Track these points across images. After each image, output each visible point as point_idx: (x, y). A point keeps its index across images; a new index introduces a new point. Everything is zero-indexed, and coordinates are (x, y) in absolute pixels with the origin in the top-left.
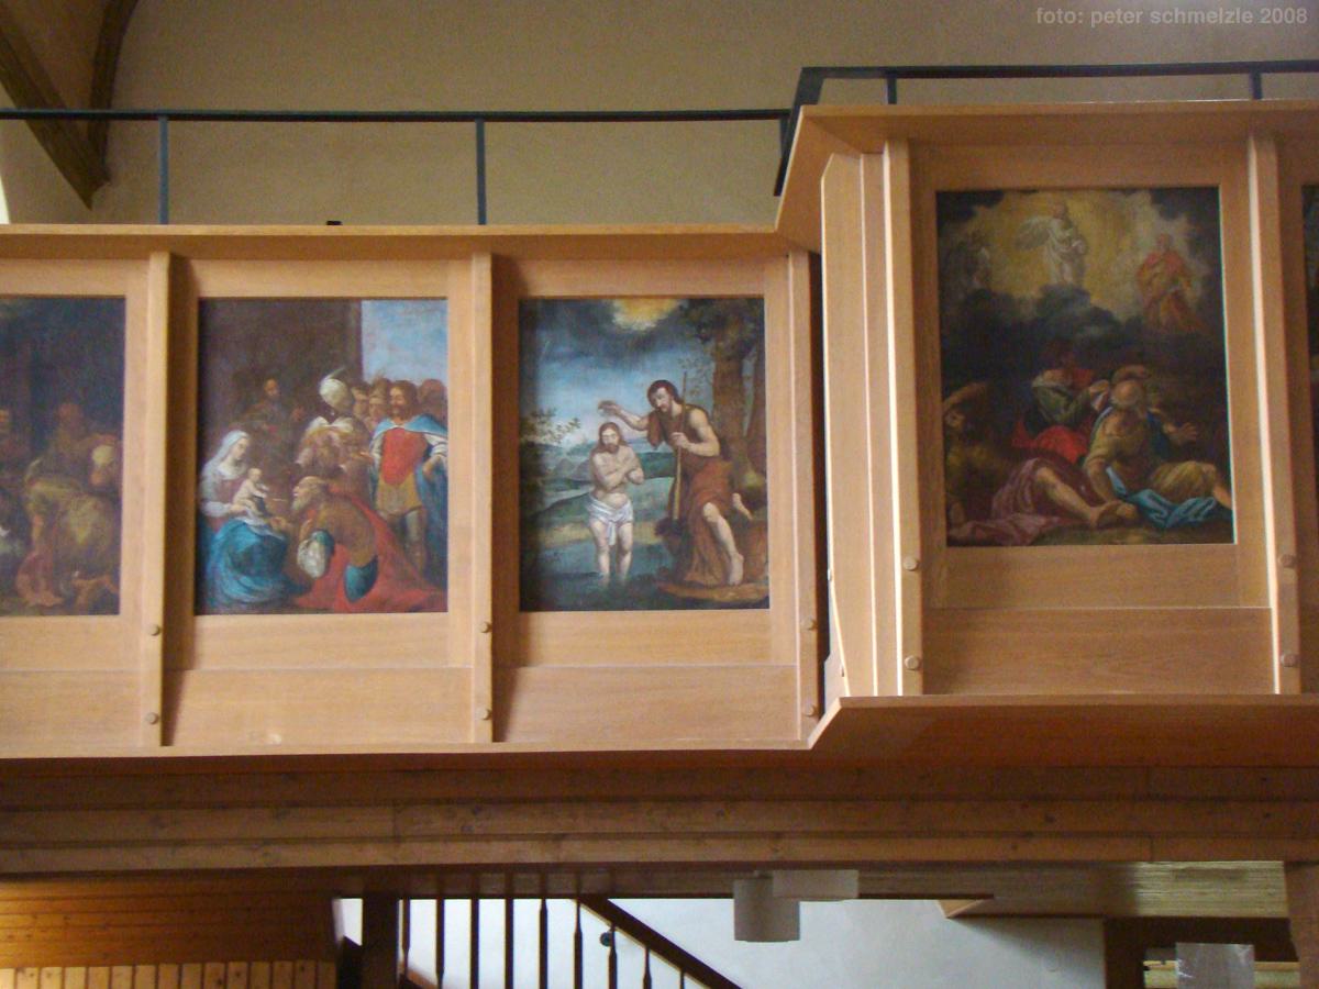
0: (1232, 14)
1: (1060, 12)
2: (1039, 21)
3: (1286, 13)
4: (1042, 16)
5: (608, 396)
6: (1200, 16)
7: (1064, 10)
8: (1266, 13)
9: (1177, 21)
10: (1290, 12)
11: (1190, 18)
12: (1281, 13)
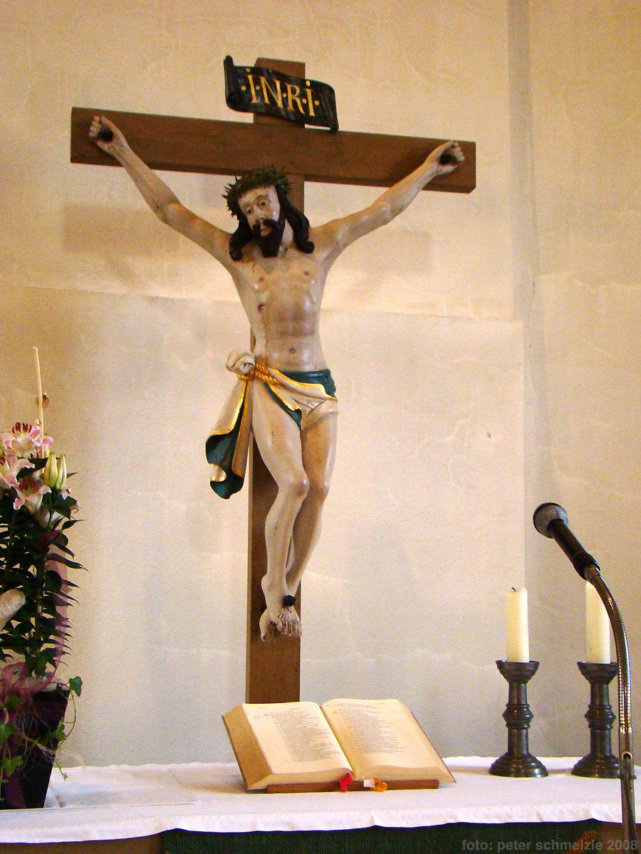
0: (589, 844)
1: (516, 843)
2: (464, 849)
3: (621, 846)
4: (466, 845)
5: (308, 269)
6: (568, 845)
7: (519, 842)
8: (611, 843)
9: (553, 849)
10: (626, 843)
11: (562, 846)
12: (621, 843)
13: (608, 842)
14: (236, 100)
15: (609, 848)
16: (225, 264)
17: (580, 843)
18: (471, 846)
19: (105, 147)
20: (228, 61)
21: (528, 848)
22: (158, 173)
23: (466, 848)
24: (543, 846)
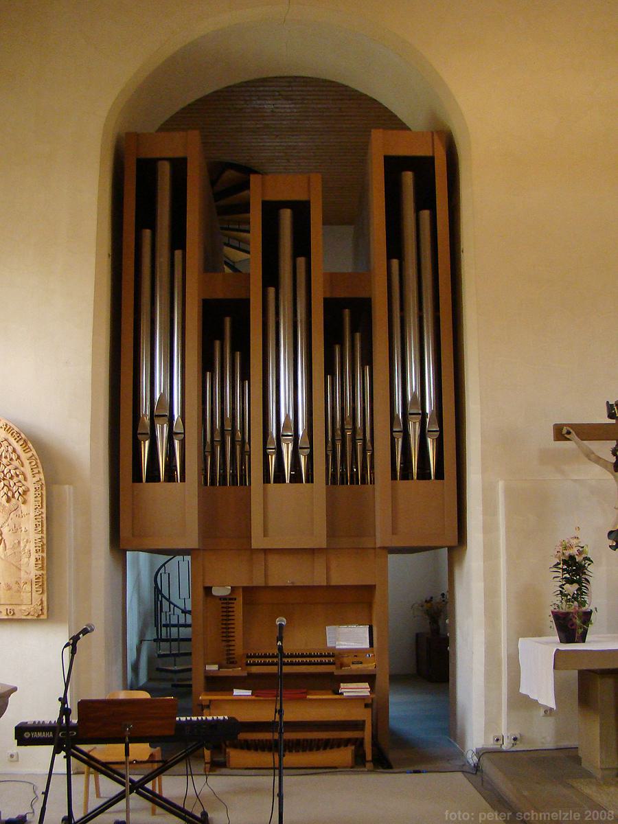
2: (447, 819)
3: (601, 813)
4: (449, 815)
6: (547, 815)
8: (588, 814)
12: (598, 813)
13: (586, 813)
14: (611, 415)
15: (586, 819)
16: (612, 473)
17: (558, 813)
18: (453, 816)
19: (568, 436)
20: (608, 402)
21: (508, 819)
22: (585, 442)
23: (449, 818)
24: (523, 816)
